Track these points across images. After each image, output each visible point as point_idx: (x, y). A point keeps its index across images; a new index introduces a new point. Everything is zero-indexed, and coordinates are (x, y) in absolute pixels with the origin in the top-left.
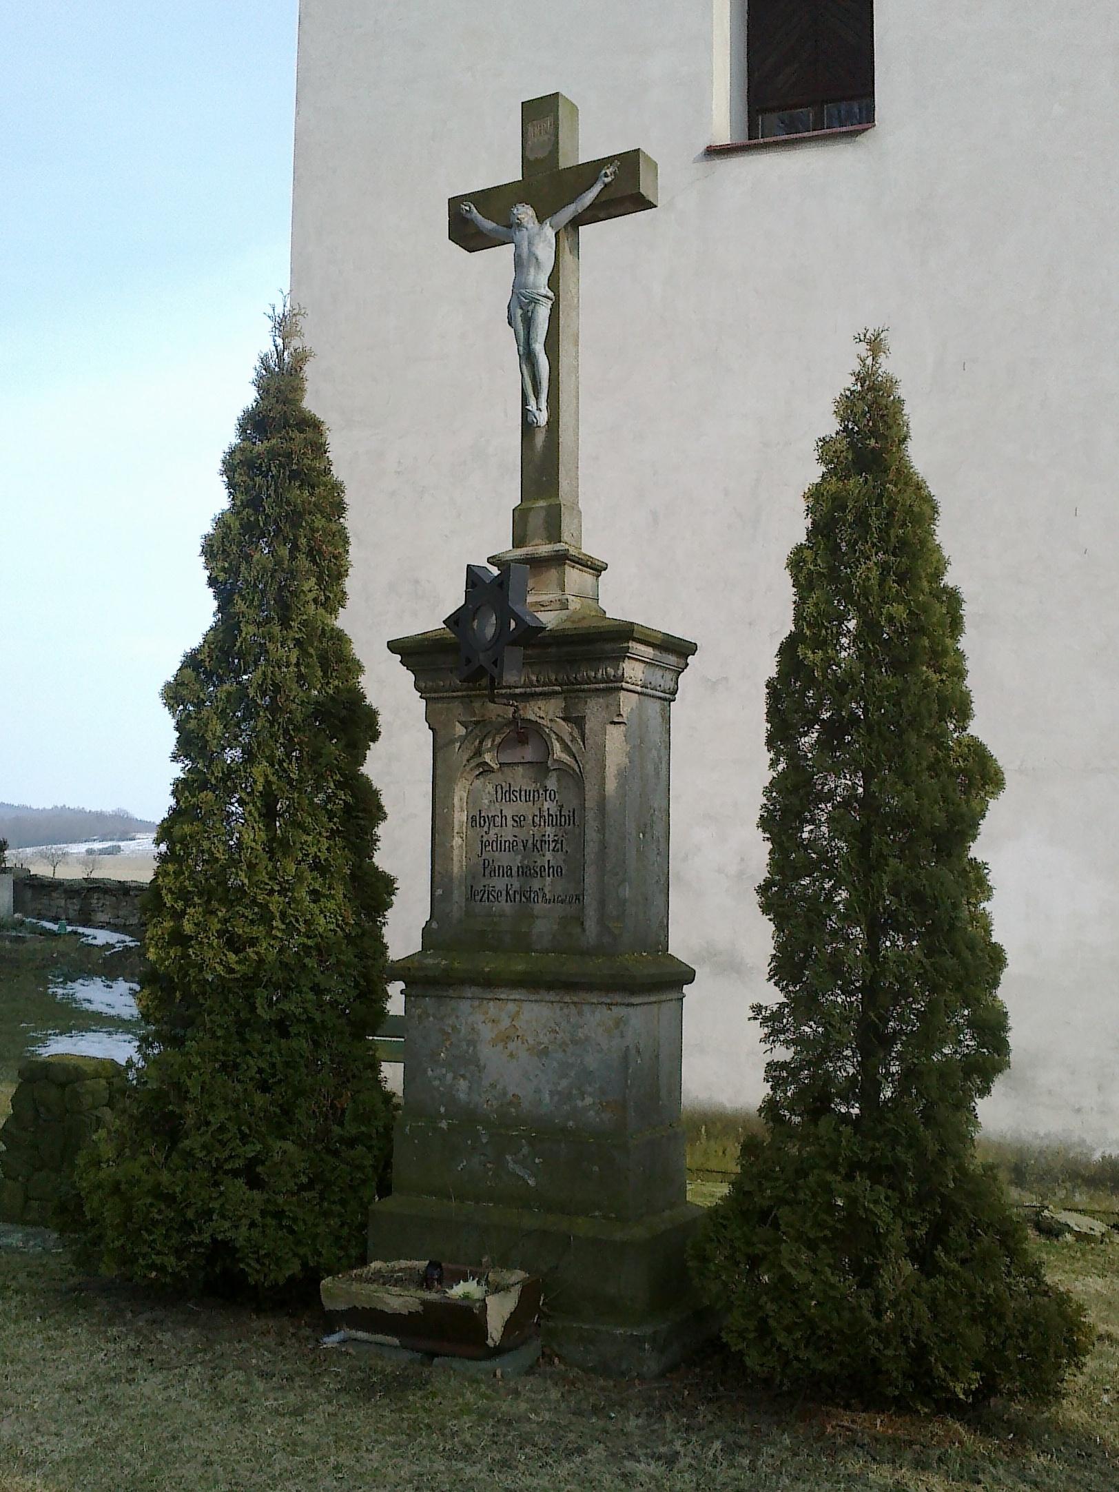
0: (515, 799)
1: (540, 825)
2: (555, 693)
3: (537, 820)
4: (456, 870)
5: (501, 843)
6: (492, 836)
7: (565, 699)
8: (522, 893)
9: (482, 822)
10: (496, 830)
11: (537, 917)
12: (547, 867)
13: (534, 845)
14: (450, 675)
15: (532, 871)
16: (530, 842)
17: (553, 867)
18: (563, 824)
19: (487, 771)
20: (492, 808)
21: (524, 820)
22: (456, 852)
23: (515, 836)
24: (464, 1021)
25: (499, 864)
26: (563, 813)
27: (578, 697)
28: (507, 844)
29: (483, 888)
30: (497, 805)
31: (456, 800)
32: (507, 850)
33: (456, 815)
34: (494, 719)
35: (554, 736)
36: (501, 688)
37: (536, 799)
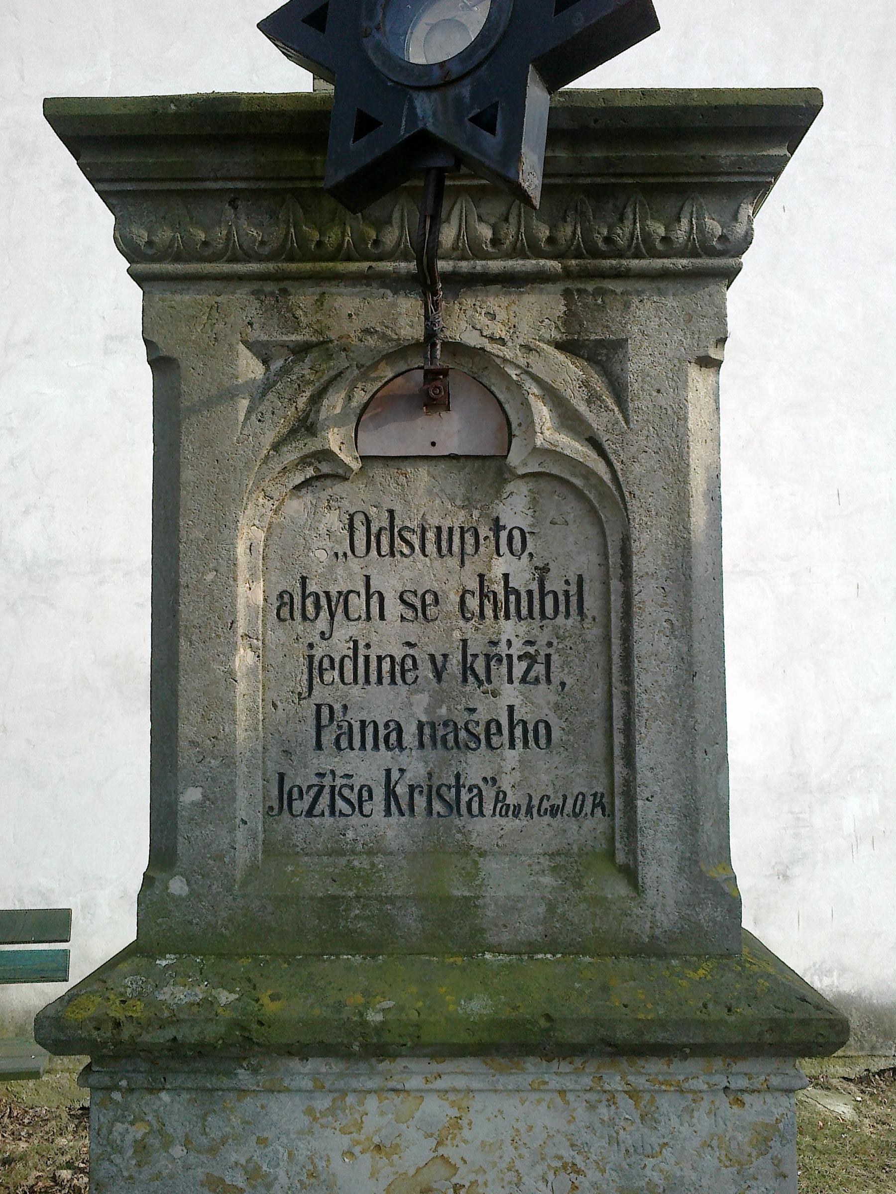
0: (406, 551)
1: (482, 615)
2: (541, 278)
3: (473, 603)
4: (241, 734)
5: (367, 658)
6: (340, 646)
7: (567, 293)
8: (433, 792)
9: (310, 608)
10: (353, 629)
11: (482, 854)
12: (505, 723)
13: (467, 669)
14: (229, 211)
15: (463, 734)
16: (455, 659)
17: (525, 723)
18: (549, 611)
19: (326, 476)
20: (340, 571)
21: (437, 602)
22: (242, 687)
23: (409, 644)
24: (283, 1154)
25: (364, 715)
26: (548, 588)
27: (600, 292)
28: (386, 666)
29: (315, 780)
30: (354, 564)
31: (241, 548)
32: (386, 679)
33: (242, 588)
34: (355, 341)
35: (533, 389)
36: (380, 259)
37: (469, 549)
